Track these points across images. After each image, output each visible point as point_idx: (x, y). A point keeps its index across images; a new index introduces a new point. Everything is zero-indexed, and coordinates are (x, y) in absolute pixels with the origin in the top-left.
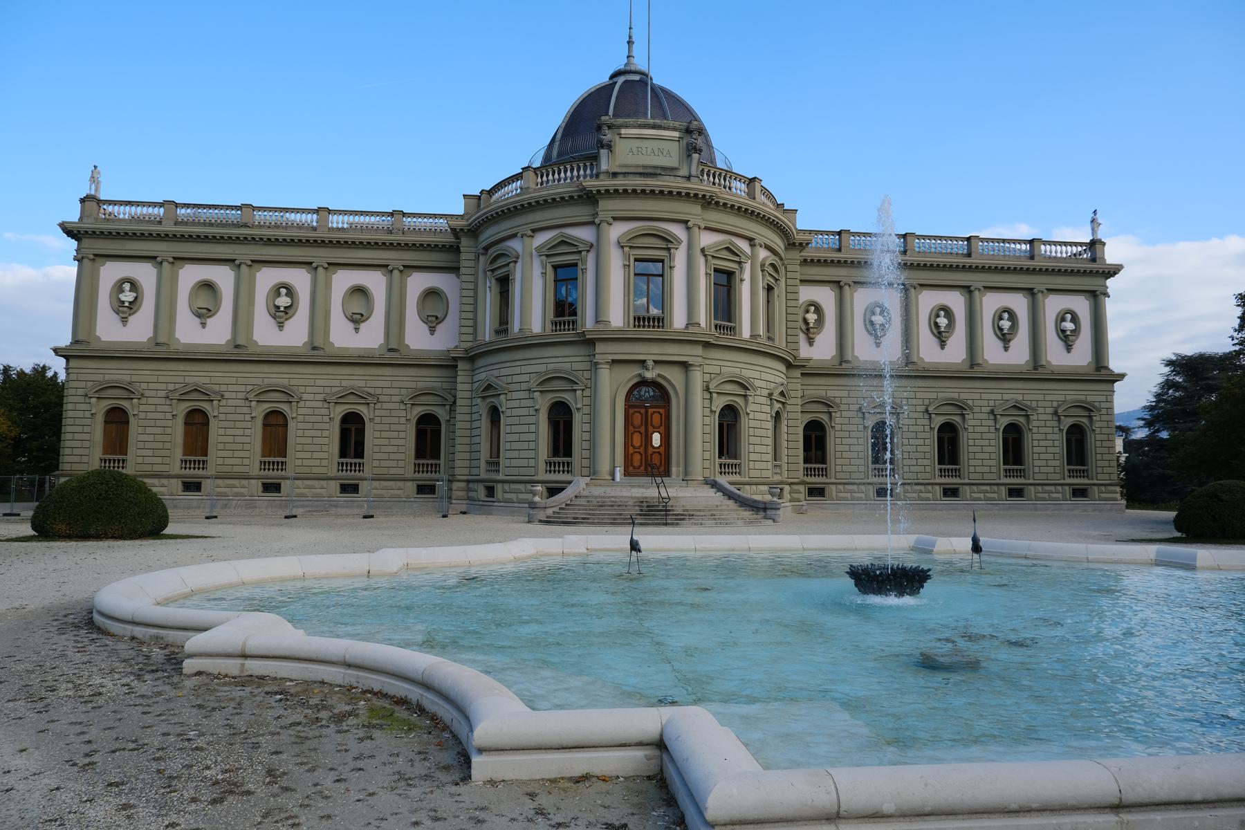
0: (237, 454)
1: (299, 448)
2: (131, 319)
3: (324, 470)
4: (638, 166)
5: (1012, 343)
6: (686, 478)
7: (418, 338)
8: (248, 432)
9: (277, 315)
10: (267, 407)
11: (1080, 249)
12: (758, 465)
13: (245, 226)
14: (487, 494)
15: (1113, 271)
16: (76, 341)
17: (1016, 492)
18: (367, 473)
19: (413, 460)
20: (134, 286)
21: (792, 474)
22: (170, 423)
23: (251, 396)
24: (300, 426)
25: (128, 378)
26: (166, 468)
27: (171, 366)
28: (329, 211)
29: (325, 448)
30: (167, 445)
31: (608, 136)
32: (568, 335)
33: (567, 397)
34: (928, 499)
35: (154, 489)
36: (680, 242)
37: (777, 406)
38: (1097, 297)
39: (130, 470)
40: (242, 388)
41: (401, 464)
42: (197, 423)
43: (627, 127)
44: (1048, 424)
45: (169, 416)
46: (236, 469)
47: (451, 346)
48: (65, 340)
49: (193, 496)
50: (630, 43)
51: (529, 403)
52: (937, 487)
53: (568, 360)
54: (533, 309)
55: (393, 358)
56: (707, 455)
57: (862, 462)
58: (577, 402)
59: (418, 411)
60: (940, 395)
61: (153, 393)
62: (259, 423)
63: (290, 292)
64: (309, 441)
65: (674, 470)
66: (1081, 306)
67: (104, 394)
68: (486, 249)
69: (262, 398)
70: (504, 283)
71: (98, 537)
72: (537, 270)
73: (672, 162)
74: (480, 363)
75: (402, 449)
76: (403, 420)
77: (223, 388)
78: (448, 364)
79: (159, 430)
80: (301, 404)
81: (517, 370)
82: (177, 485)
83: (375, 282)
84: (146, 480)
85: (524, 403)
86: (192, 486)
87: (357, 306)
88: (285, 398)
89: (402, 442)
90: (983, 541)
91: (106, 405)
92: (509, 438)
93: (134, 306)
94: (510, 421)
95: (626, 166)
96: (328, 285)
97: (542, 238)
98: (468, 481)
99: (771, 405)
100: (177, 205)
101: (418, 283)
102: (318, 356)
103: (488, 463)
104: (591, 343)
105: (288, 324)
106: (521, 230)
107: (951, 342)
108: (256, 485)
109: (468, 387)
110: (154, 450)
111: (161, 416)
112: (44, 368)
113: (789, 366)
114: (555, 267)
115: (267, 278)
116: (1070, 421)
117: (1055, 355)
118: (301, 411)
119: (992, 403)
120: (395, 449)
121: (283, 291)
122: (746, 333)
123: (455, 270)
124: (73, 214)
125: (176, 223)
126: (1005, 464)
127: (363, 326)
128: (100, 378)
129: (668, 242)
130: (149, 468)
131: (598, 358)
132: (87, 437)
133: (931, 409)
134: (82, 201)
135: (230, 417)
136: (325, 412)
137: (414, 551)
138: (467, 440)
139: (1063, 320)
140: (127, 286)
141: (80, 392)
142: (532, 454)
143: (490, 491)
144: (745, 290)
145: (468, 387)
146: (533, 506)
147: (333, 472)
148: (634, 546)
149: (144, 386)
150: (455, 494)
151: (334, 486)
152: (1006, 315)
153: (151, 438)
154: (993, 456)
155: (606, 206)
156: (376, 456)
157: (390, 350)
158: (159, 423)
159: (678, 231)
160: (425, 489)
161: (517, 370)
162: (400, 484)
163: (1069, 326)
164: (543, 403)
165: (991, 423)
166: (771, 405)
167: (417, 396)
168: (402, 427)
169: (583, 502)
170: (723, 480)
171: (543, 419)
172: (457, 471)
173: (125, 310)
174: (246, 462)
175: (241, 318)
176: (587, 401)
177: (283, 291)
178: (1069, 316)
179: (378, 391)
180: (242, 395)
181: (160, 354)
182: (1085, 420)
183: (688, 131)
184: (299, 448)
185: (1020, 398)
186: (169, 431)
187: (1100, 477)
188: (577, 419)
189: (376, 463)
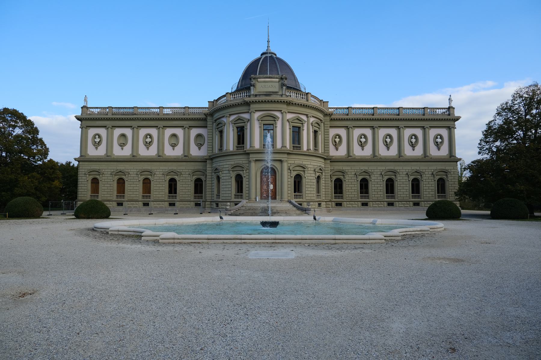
0: (134, 193)
1: (155, 191)
2: (99, 148)
3: (163, 198)
4: (264, 92)
5: (416, 148)
6: (281, 200)
7: (195, 152)
8: (138, 186)
9: (146, 145)
10: (144, 177)
11: (444, 110)
12: (309, 195)
13: (135, 114)
14: (216, 206)
15: (458, 119)
16: (81, 156)
17: (391, 204)
18: (178, 199)
19: (193, 195)
20: (99, 136)
21: (327, 198)
22: (112, 183)
23: (138, 173)
24: (155, 183)
25: (98, 168)
26: (111, 198)
27: (112, 163)
28: (163, 108)
29: (163, 191)
30: (112, 190)
31: (253, 82)
32: (241, 151)
33: (241, 173)
34: (376, 207)
35: (108, 205)
36: (279, 118)
37: (318, 174)
38: (450, 129)
39: (99, 199)
40: (135, 170)
41: (190, 196)
42: (121, 183)
43: (260, 78)
44: (430, 178)
45: (112, 180)
46: (134, 198)
47: (206, 155)
48: (78, 155)
49: (120, 208)
50: (268, 41)
51: (229, 175)
52: (385, 203)
53: (240, 160)
54: (230, 143)
55: (186, 159)
56: (289, 192)
57: (356, 193)
58: (244, 174)
59: (195, 177)
60: (387, 168)
61: (106, 173)
62: (141, 182)
63: (151, 137)
64: (158, 188)
65: (277, 197)
66: (444, 132)
67: (90, 174)
68: (216, 120)
69: (142, 174)
70: (221, 132)
71: (92, 218)
72: (231, 129)
73: (276, 90)
74: (214, 160)
75: (190, 191)
76: (190, 181)
77: (129, 170)
78: (204, 161)
79: (109, 185)
80: (155, 176)
81: (225, 163)
82: (115, 204)
83: (179, 132)
84: (105, 203)
85: (227, 175)
86: (120, 204)
87: (173, 141)
88: (150, 174)
89: (190, 188)
90: (317, 218)
91: (92, 177)
92: (223, 187)
93: (100, 143)
94: (223, 181)
95: (260, 92)
96: (163, 134)
97: (233, 118)
98: (211, 202)
99: (315, 174)
100: (112, 108)
101: (194, 132)
102: (161, 159)
103: (217, 195)
104: (248, 154)
105: (150, 148)
106: (225, 115)
107: (391, 148)
108: (141, 204)
109: (210, 169)
110: (107, 192)
111: (109, 180)
112: (70, 163)
113: (325, 159)
114: (237, 128)
115: (143, 132)
116: (438, 177)
117: (433, 152)
118: (155, 178)
119: (407, 171)
120: (187, 191)
121: (148, 136)
122: (305, 148)
123: (206, 127)
124: (79, 113)
125: (113, 114)
126: (386, 193)
127: (175, 148)
128: (89, 168)
129: (275, 118)
130: (105, 198)
131: (251, 159)
132: (86, 188)
133: (383, 173)
134: (82, 108)
135: (132, 180)
136: (163, 178)
137: (168, 219)
138: (210, 187)
139: (437, 138)
140: (97, 137)
141: (83, 173)
142: (230, 192)
143: (217, 205)
144: (305, 134)
145: (210, 169)
146: (227, 210)
147: (166, 199)
148: (221, 218)
149: (104, 170)
150: (207, 206)
151: (167, 204)
152: (413, 137)
153: (106, 188)
154: (407, 191)
155: (252, 106)
156: (181, 193)
157: (185, 156)
158: (109, 183)
159: (278, 114)
160: (198, 205)
161: (225, 163)
162: (189, 203)
163: (439, 140)
164: (233, 175)
165: (407, 178)
166: (315, 174)
167: (194, 172)
168: (190, 183)
169: (244, 208)
170: (293, 201)
171: (233, 180)
172: (207, 198)
173: (97, 145)
174: (137, 196)
175: (135, 146)
176: (247, 174)
177: (148, 136)
178: (439, 137)
179: (181, 171)
180: (135, 173)
181: (108, 159)
182: (445, 177)
183: (282, 79)
184: (155, 191)
185: (418, 168)
186: (112, 185)
187: (450, 198)
188: (244, 179)
189: (181, 196)
